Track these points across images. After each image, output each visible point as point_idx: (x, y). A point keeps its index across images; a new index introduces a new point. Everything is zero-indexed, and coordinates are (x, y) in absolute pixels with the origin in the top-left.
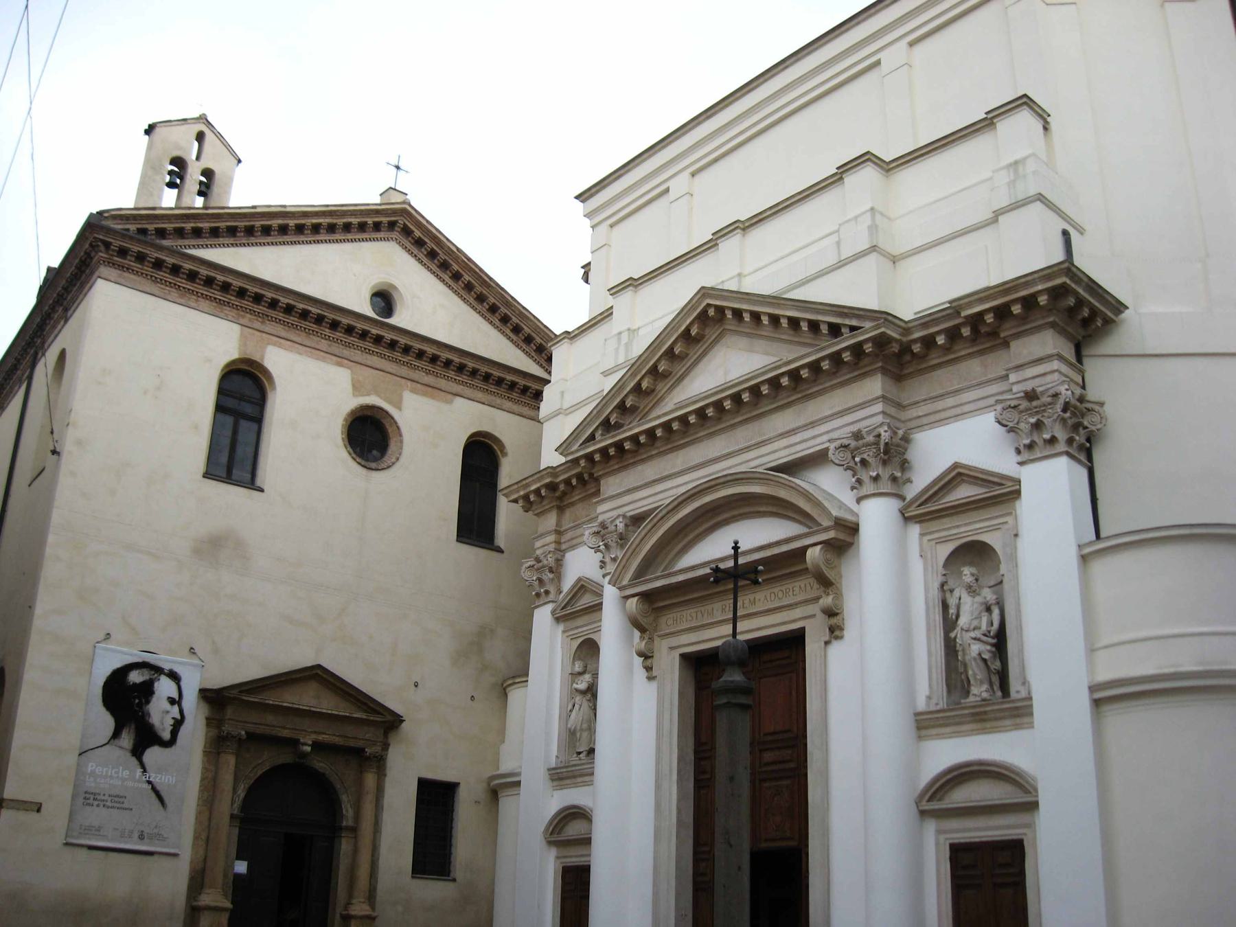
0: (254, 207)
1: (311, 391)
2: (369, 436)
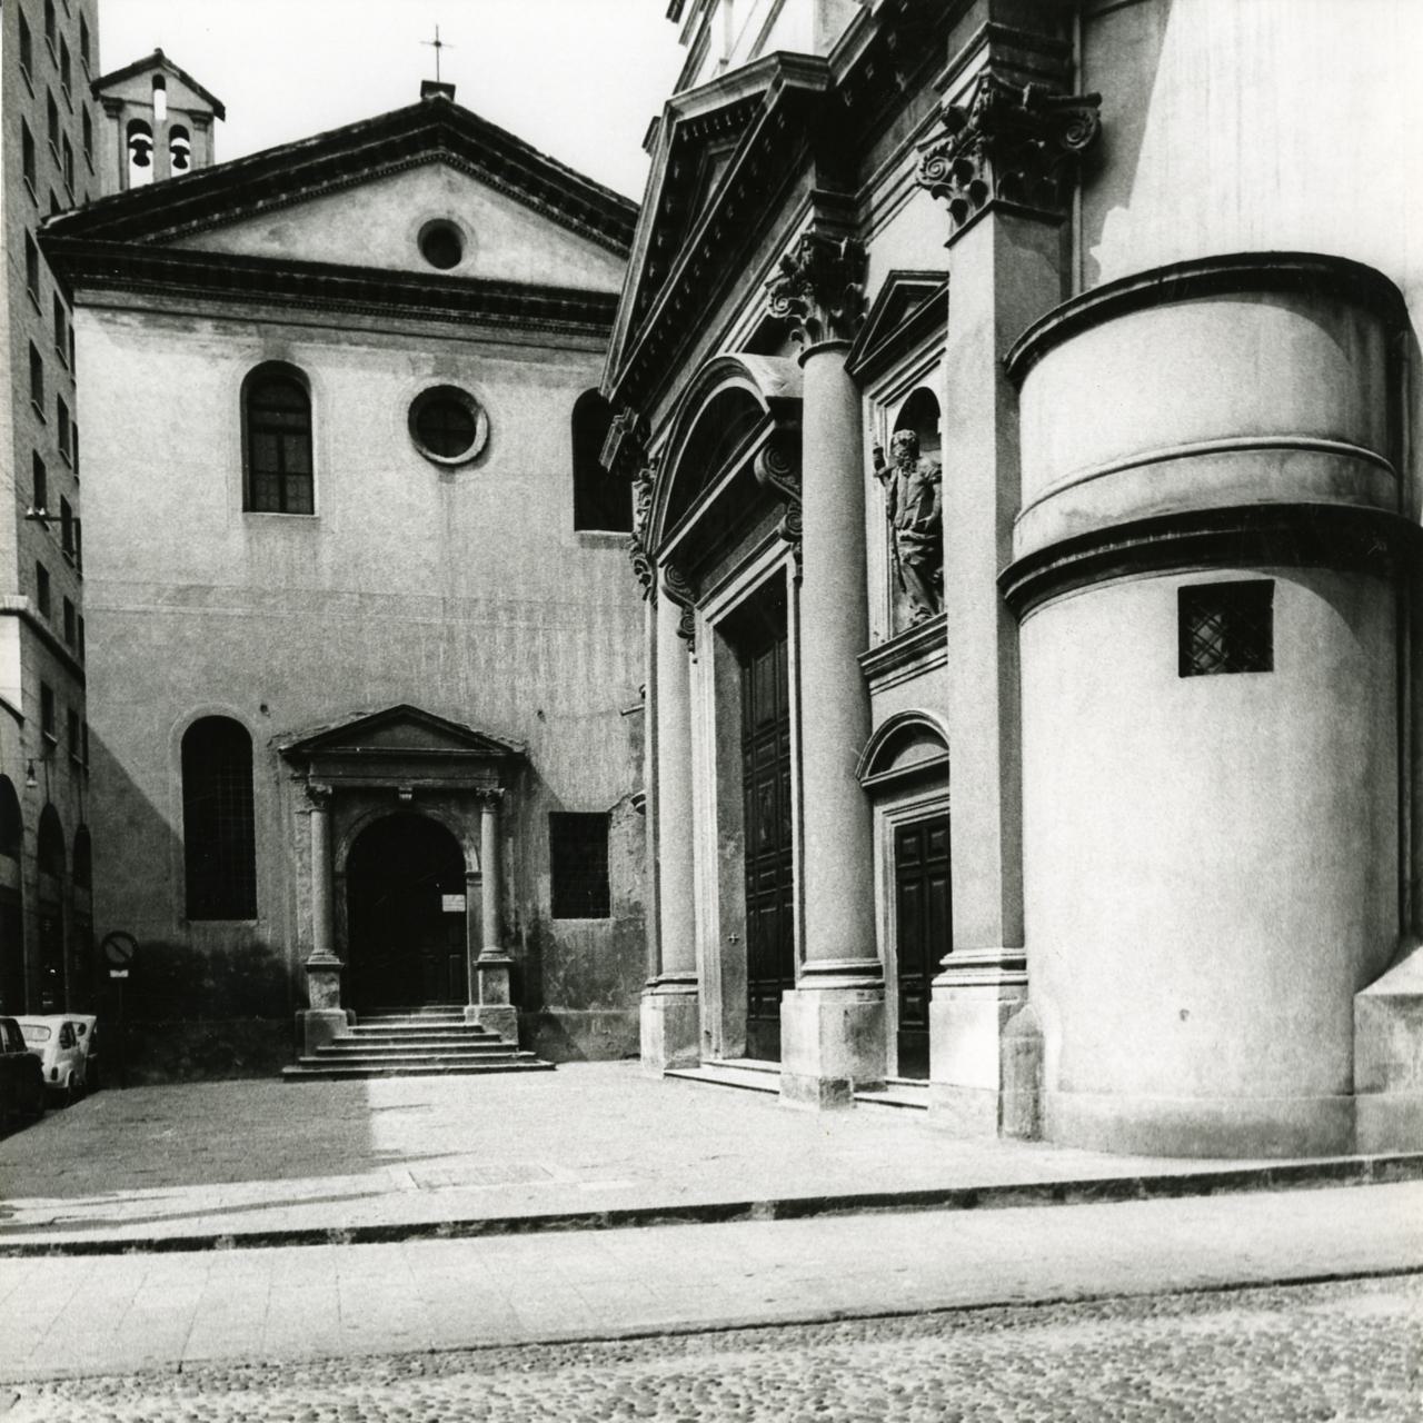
0: (303, 142)
1: (360, 395)
2: (443, 425)
